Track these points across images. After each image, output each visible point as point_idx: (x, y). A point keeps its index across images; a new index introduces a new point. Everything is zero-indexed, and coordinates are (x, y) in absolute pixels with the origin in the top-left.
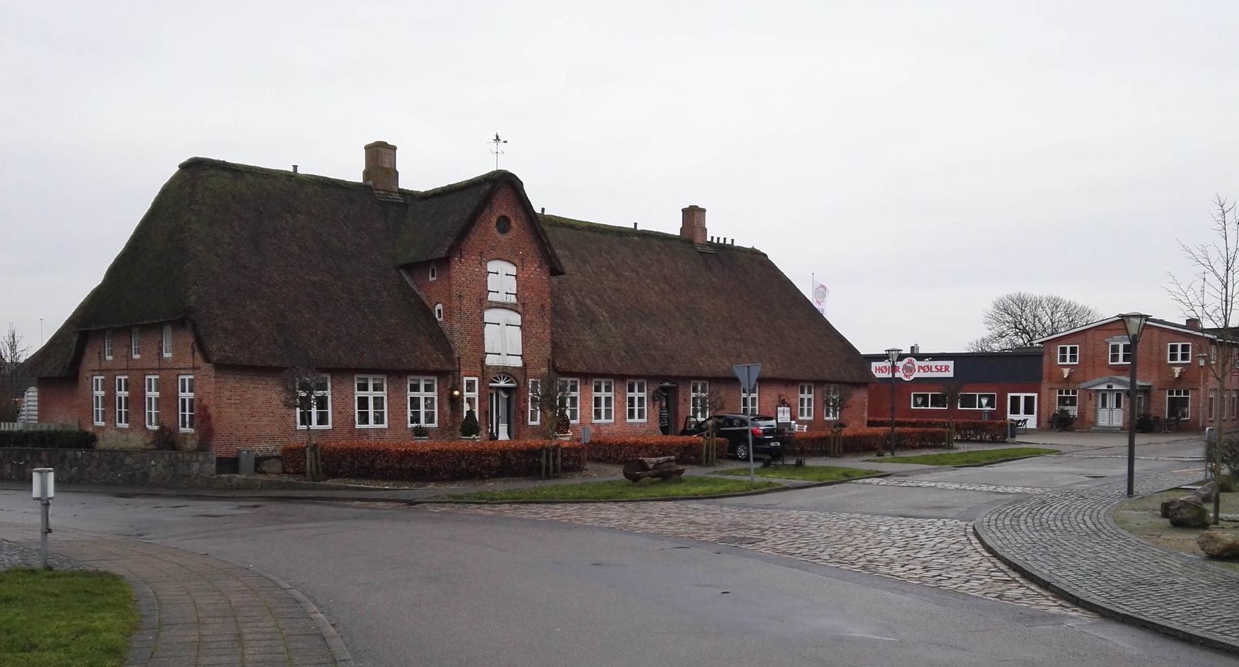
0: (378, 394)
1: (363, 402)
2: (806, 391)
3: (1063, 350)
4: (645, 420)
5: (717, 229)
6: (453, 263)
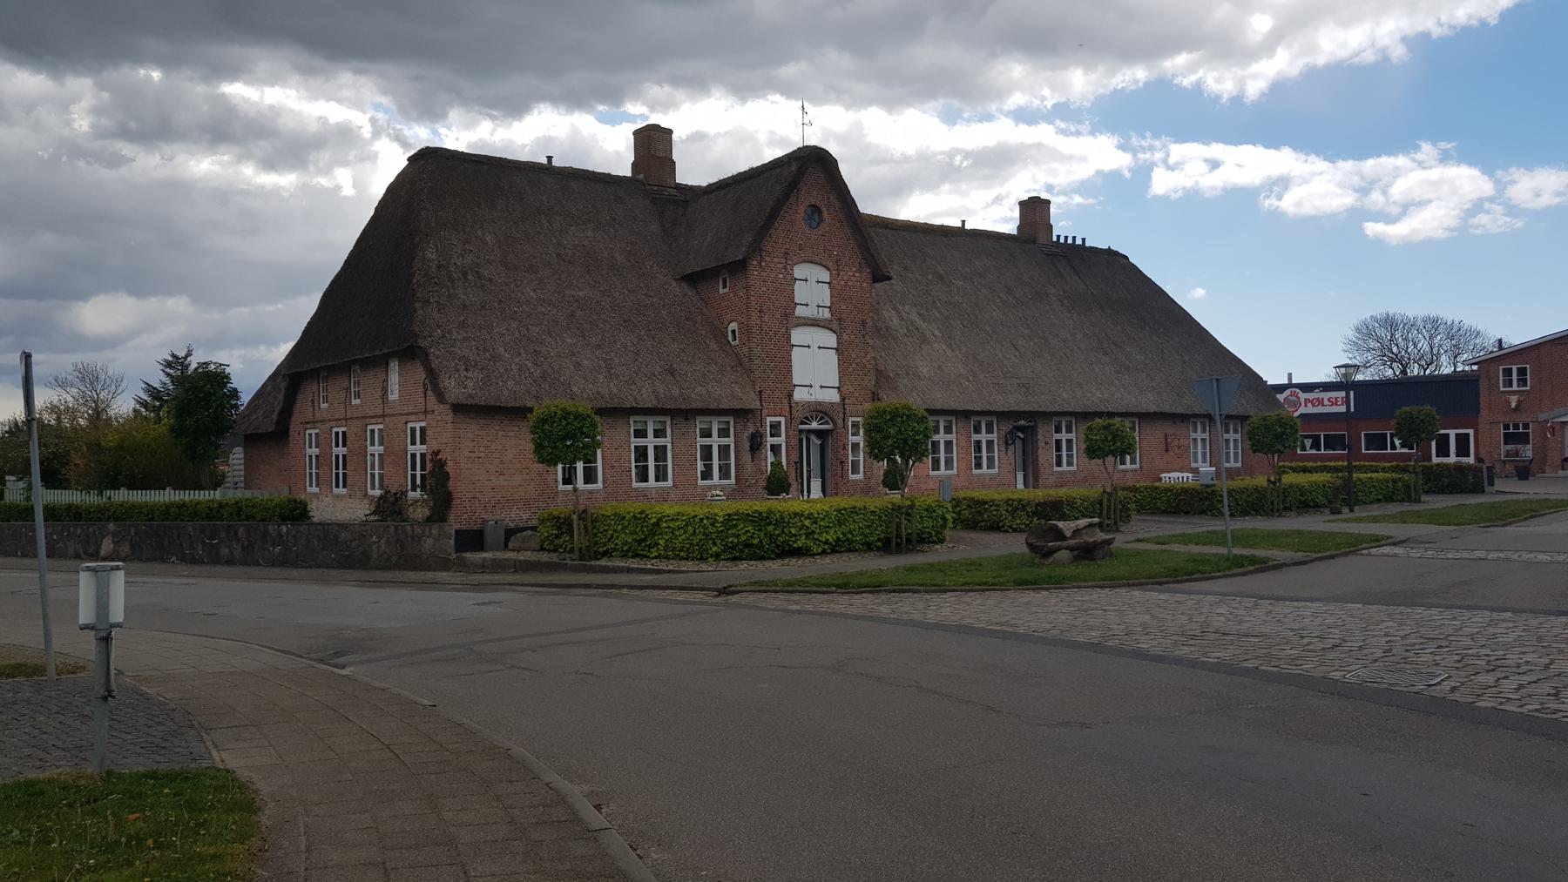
0: (660, 441)
1: (641, 453)
2: (1199, 430)
3: (1508, 372)
4: (996, 470)
5: (1063, 226)
6: (751, 267)
